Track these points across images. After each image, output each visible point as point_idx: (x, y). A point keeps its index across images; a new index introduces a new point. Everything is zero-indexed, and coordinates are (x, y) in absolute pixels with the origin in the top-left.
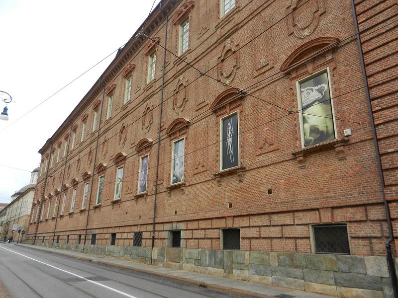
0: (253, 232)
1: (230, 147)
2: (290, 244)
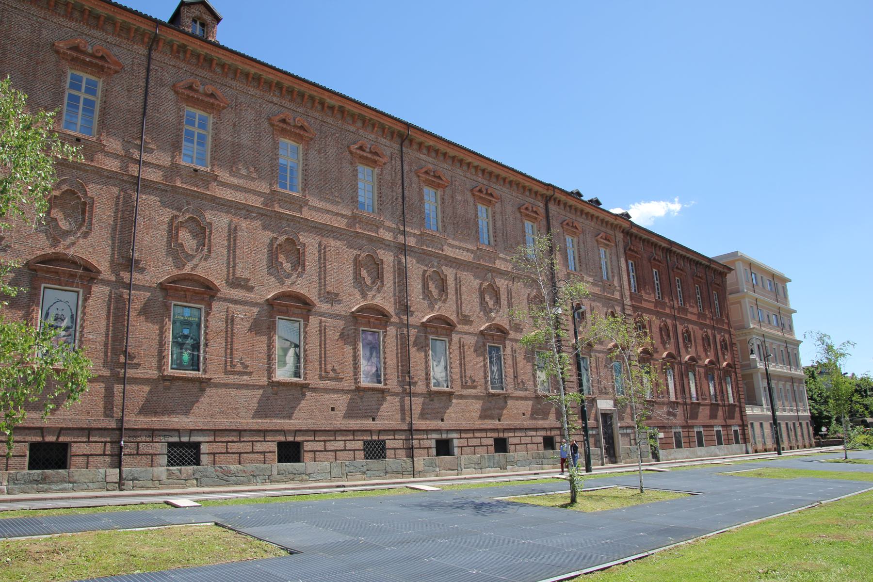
0: (517, 440)
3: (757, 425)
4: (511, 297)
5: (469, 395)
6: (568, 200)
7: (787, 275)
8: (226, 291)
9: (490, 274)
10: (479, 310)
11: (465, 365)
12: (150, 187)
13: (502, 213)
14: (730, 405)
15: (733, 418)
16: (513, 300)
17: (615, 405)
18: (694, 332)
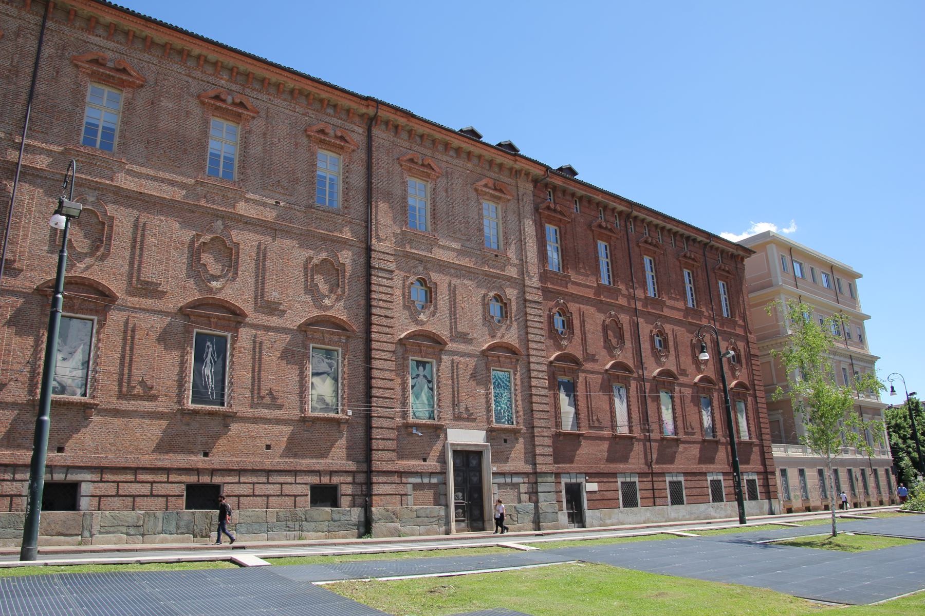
1: (208, 377)
2: (289, 501)
3: (793, 474)
4: (264, 260)
5: (136, 411)
6: (411, 124)
7: (856, 269)
8: (253, 317)
9: (219, 223)
10: (183, 275)
11: (131, 360)
12: (31, 175)
13: (265, 134)
14: (616, 438)
15: (711, 460)
16: (268, 264)
17: (489, 438)
18: (675, 336)
